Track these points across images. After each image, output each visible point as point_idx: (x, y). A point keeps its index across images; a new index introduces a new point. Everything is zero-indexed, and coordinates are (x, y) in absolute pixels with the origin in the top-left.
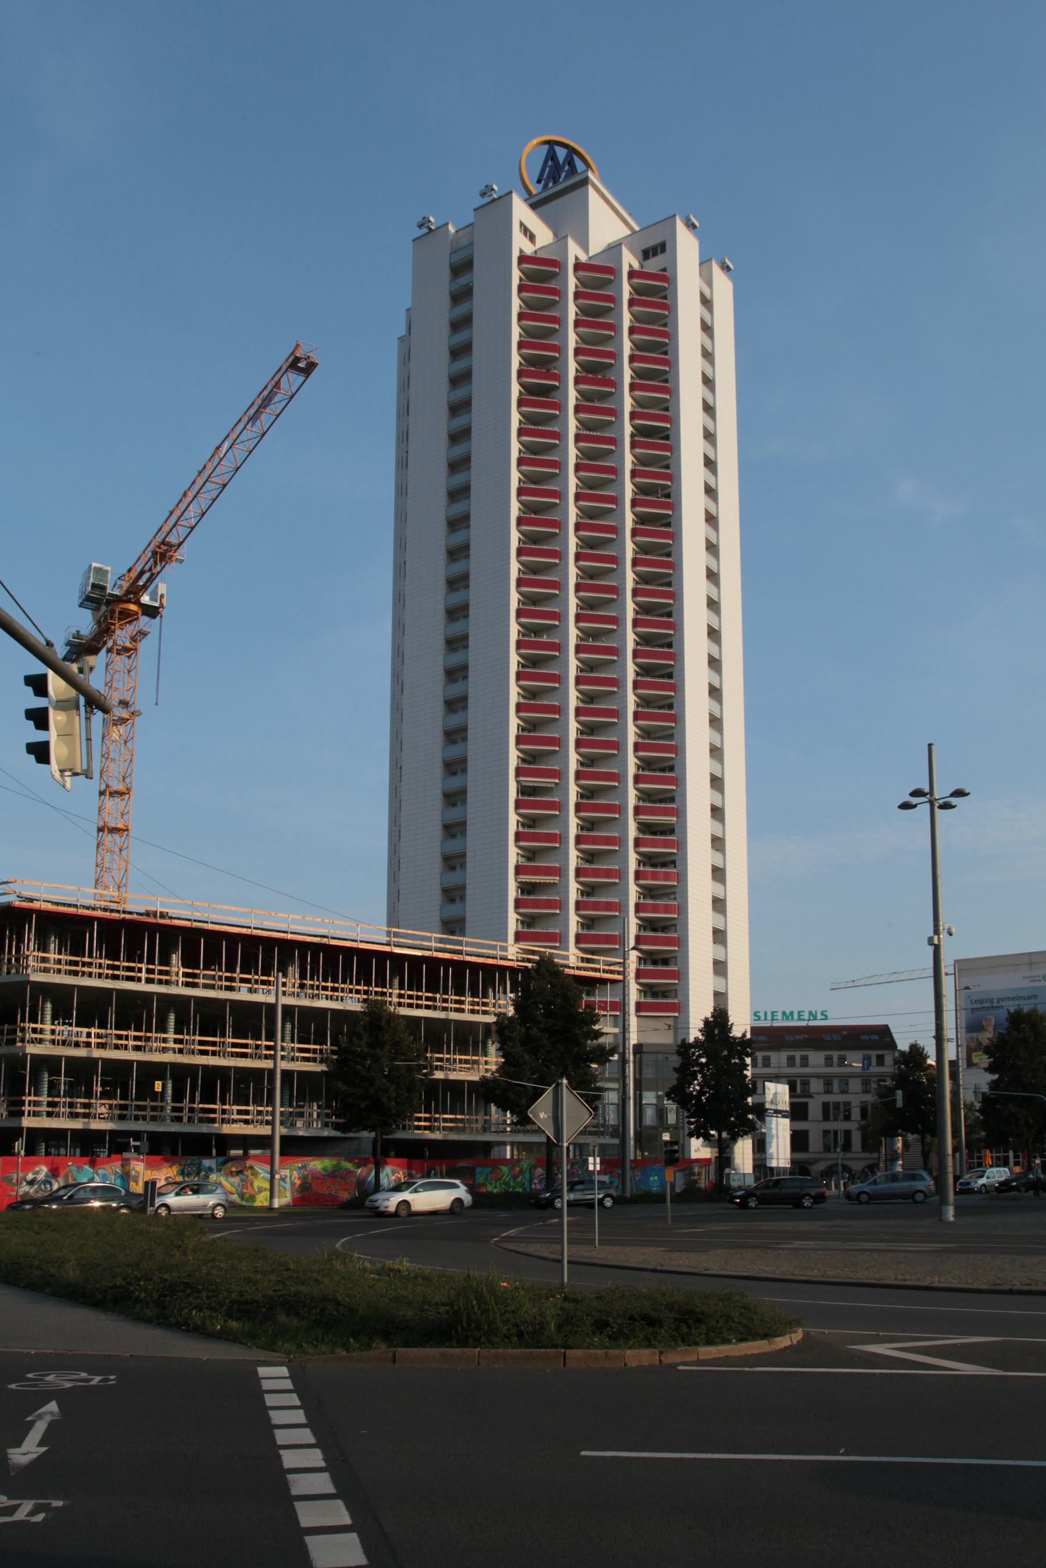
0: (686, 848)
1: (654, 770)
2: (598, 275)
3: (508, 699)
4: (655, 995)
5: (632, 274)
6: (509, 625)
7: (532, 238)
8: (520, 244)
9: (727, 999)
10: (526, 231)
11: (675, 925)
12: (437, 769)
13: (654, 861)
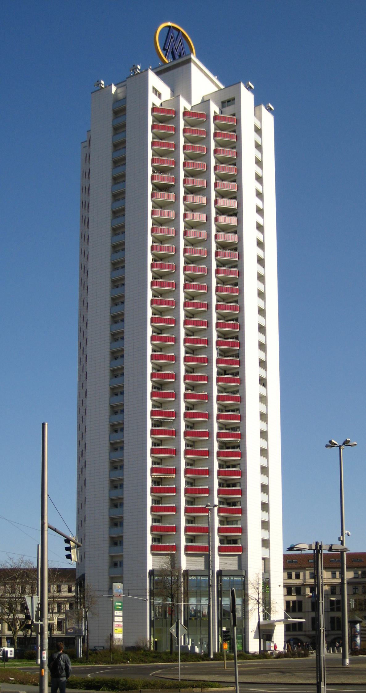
0: (247, 552)
1: (228, 338)
2: (197, 117)
3: (147, 333)
4: (229, 542)
5: (215, 118)
6: (147, 383)
7: (159, 96)
8: (153, 100)
9: (270, 561)
10: (155, 91)
11: (239, 464)
12: (107, 320)
13: (227, 427)
